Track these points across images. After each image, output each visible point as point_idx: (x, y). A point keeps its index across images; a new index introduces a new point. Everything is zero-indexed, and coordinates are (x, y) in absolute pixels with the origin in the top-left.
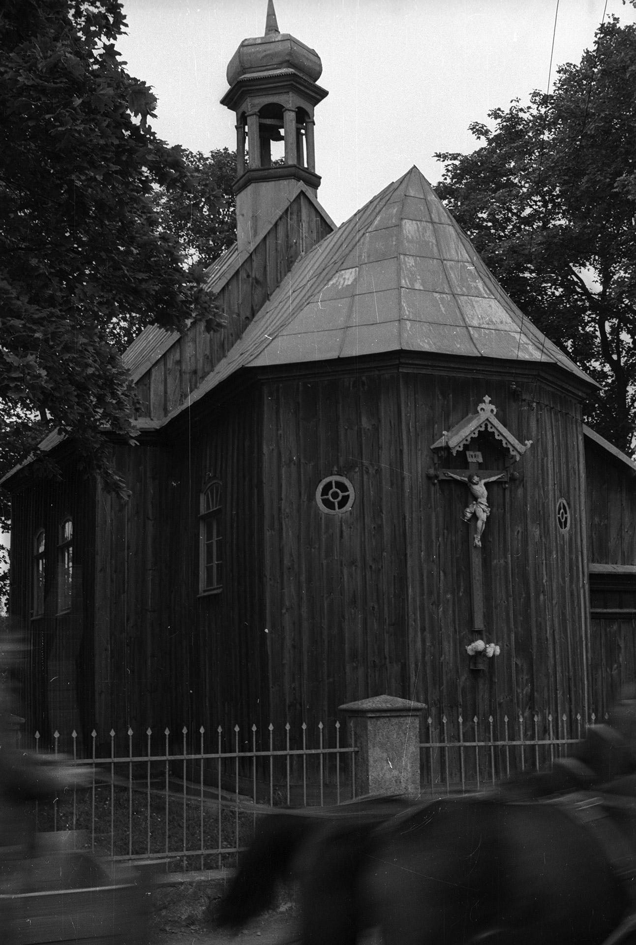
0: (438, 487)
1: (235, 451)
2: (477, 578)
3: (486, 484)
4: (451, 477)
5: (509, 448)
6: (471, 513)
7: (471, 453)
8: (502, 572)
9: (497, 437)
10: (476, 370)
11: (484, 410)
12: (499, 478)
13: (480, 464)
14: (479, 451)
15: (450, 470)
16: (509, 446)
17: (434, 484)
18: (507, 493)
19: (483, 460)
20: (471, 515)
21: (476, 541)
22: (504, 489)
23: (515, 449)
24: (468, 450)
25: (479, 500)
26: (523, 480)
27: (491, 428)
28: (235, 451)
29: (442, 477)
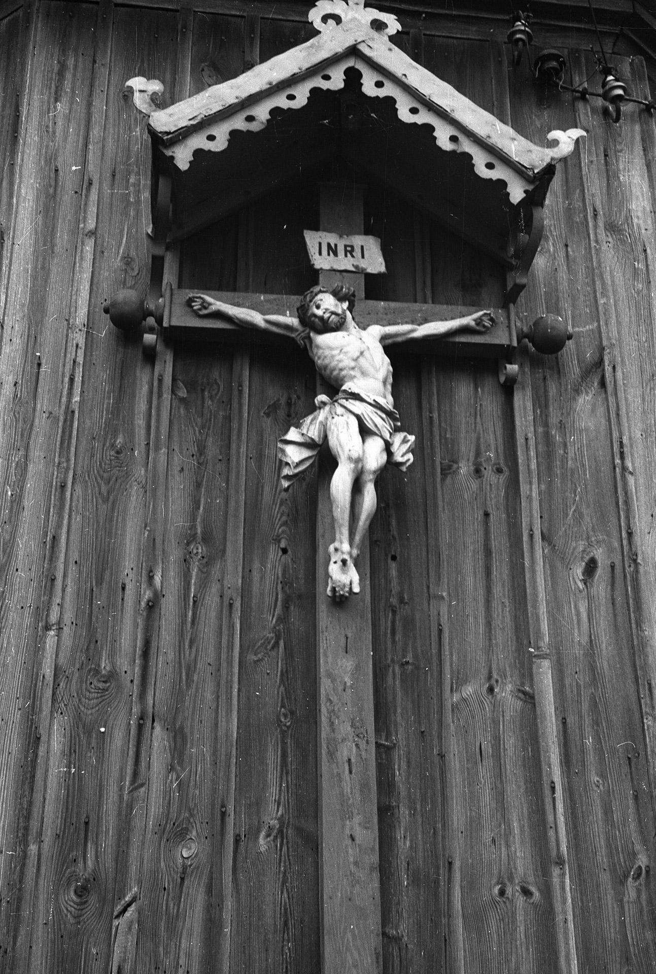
0: (166, 366)
1: (113, 933)
2: (347, 750)
3: (392, 348)
4: (219, 315)
5: (469, 157)
6: (309, 444)
7: (331, 238)
8: (511, 743)
9: (404, 115)
10: (623, 379)
11: (337, 19)
12: (464, 330)
13: (370, 279)
14: (367, 232)
15: (210, 292)
16: (467, 147)
17: (150, 356)
18: (523, 402)
19: (386, 267)
20: (305, 453)
21: (334, 570)
22: (508, 389)
23: (497, 155)
24: (316, 228)
25: (347, 386)
26: (599, 363)
27: (379, 84)
28: (113, 933)
29: (179, 318)
